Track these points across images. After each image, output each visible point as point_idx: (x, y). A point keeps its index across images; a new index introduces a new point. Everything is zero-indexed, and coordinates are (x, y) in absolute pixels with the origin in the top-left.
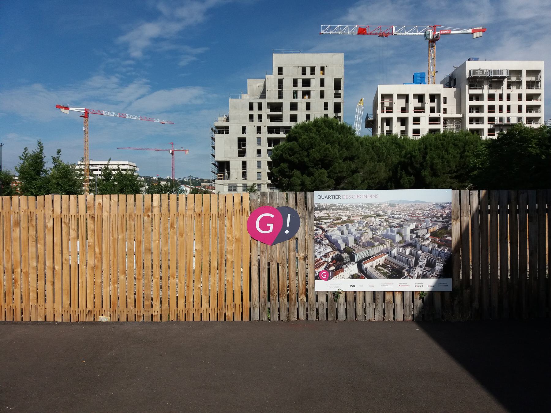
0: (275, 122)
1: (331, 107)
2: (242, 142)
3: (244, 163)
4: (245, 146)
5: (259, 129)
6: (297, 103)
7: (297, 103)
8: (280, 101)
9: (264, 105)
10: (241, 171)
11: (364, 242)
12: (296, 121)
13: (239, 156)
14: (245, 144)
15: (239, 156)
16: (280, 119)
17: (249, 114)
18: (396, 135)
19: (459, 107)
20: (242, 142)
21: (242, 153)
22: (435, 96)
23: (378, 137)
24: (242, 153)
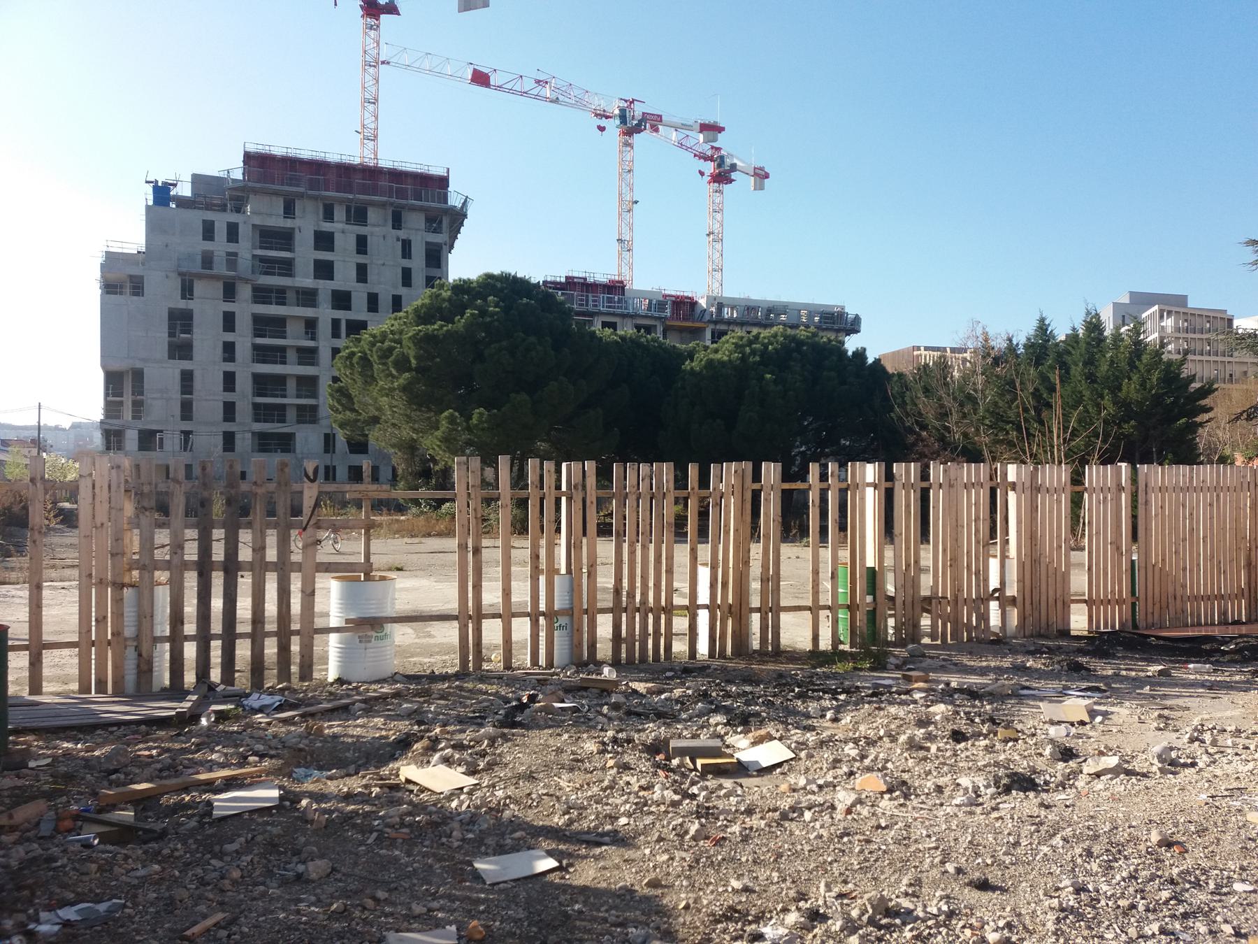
0: (273, 274)
1: (418, 251)
2: (181, 321)
3: (187, 379)
4: (189, 331)
5: (229, 322)
6: (333, 233)
7: (333, 233)
8: (289, 223)
9: (244, 231)
10: (176, 396)
11: (440, 535)
12: (330, 277)
13: (171, 357)
14: (190, 325)
15: (171, 357)
16: (287, 267)
17: (224, 312)
18: (1106, 338)
19: (587, 296)
20: (181, 321)
21: (181, 350)
22: (288, 321)
23: (1081, 335)
24: (181, 350)
